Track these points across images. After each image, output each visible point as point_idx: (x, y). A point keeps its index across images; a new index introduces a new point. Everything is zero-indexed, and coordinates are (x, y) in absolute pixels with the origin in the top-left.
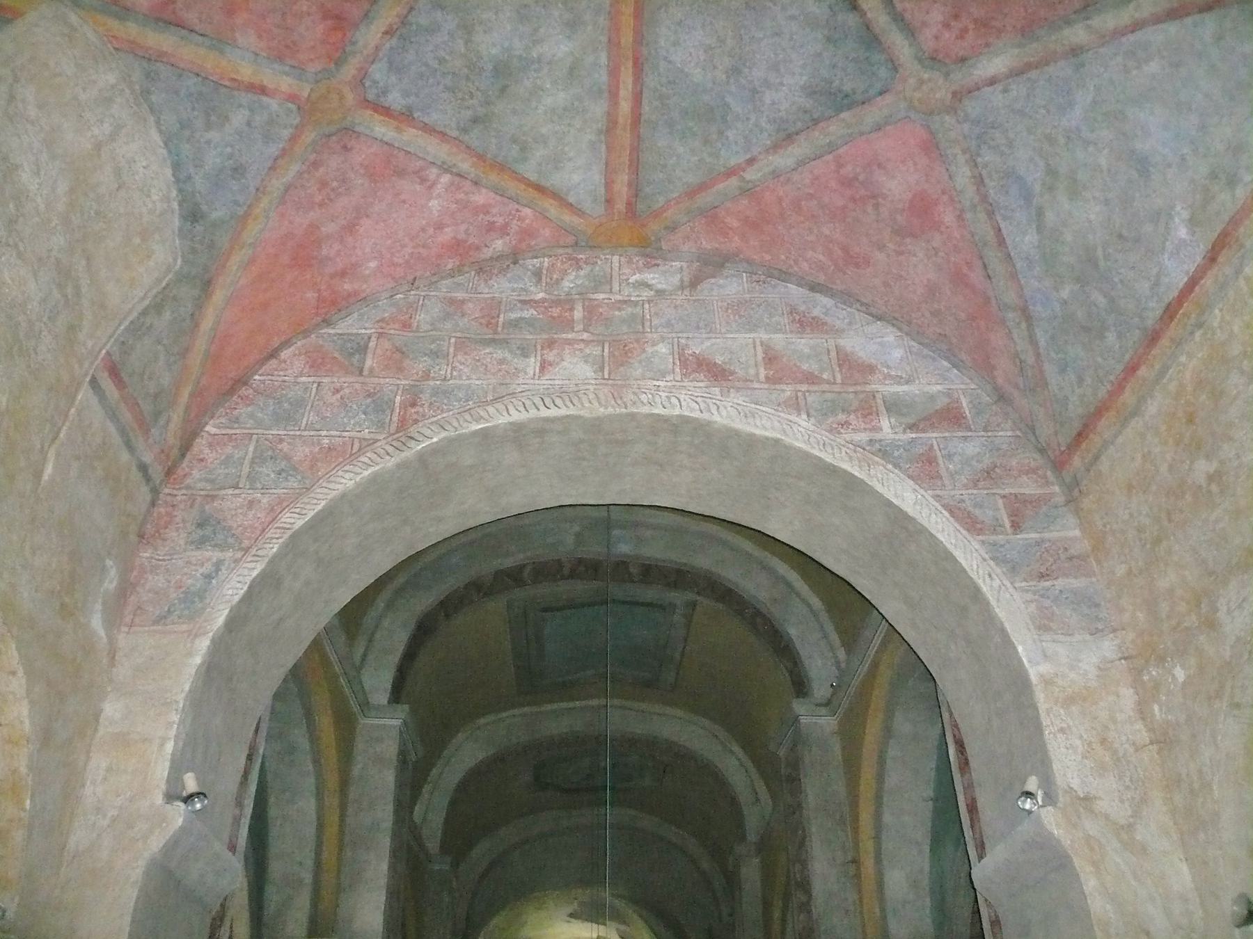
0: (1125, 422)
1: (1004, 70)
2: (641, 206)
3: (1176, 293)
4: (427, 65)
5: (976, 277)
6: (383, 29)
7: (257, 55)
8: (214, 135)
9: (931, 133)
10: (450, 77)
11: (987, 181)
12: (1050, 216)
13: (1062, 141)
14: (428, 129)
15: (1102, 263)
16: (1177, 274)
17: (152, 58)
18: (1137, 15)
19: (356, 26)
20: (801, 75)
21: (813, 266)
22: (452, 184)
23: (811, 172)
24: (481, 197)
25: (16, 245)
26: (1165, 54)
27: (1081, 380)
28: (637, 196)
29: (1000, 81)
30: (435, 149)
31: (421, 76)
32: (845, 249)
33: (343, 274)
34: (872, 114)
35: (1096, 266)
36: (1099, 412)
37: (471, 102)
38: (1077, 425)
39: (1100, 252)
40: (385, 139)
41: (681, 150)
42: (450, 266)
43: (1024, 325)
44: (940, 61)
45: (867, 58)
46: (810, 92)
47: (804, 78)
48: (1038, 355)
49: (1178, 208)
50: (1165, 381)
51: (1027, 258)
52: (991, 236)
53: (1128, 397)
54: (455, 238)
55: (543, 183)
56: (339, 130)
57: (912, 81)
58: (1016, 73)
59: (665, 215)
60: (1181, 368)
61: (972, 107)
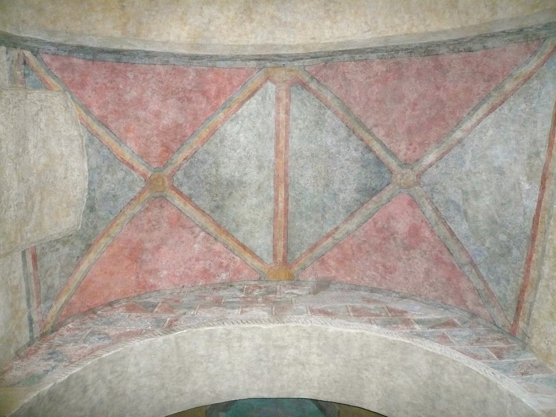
0: (536, 288)
1: (434, 159)
2: (289, 258)
3: (535, 212)
4: (199, 177)
5: (446, 257)
6: (184, 157)
7: (133, 152)
8: (109, 177)
9: (412, 196)
10: (209, 185)
11: (439, 209)
12: (470, 212)
13: (465, 177)
14: (197, 208)
15: (498, 220)
16: (531, 204)
17: (93, 134)
18: (478, 118)
19: (174, 153)
20: (354, 184)
21: (370, 279)
22: (205, 238)
23: (363, 229)
24: (218, 247)
25: (16, 164)
26: (493, 125)
27: (508, 281)
28: (287, 252)
29: (434, 164)
30: (199, 218)
31: (197, 182)
32: (384, 266)
33: (150, 272)
34: (385, 195)
35: (497, 223)
36: (522, 291)
37: (216, 198)
38: (514, 306)
39: (496, 217)
40: (178, 207)
41: (306, 226)
42: (200, 284)
43: (474, 271)
44: (408, 164)
45: (379, 171)
46: (358, 191)
47: (355, 185)
48: (484, 282)
49: (521, 178)
50: (546, 253)
51: (466, 237)
52: (448, 234)
53: (533, 274)
54: (204, 268)
55: (246, 244)
56: (160, 197)
57: (399, 176)
58: (440, 158)
59: (300, 262)
60: (551, 241)
61: (426, 179)
